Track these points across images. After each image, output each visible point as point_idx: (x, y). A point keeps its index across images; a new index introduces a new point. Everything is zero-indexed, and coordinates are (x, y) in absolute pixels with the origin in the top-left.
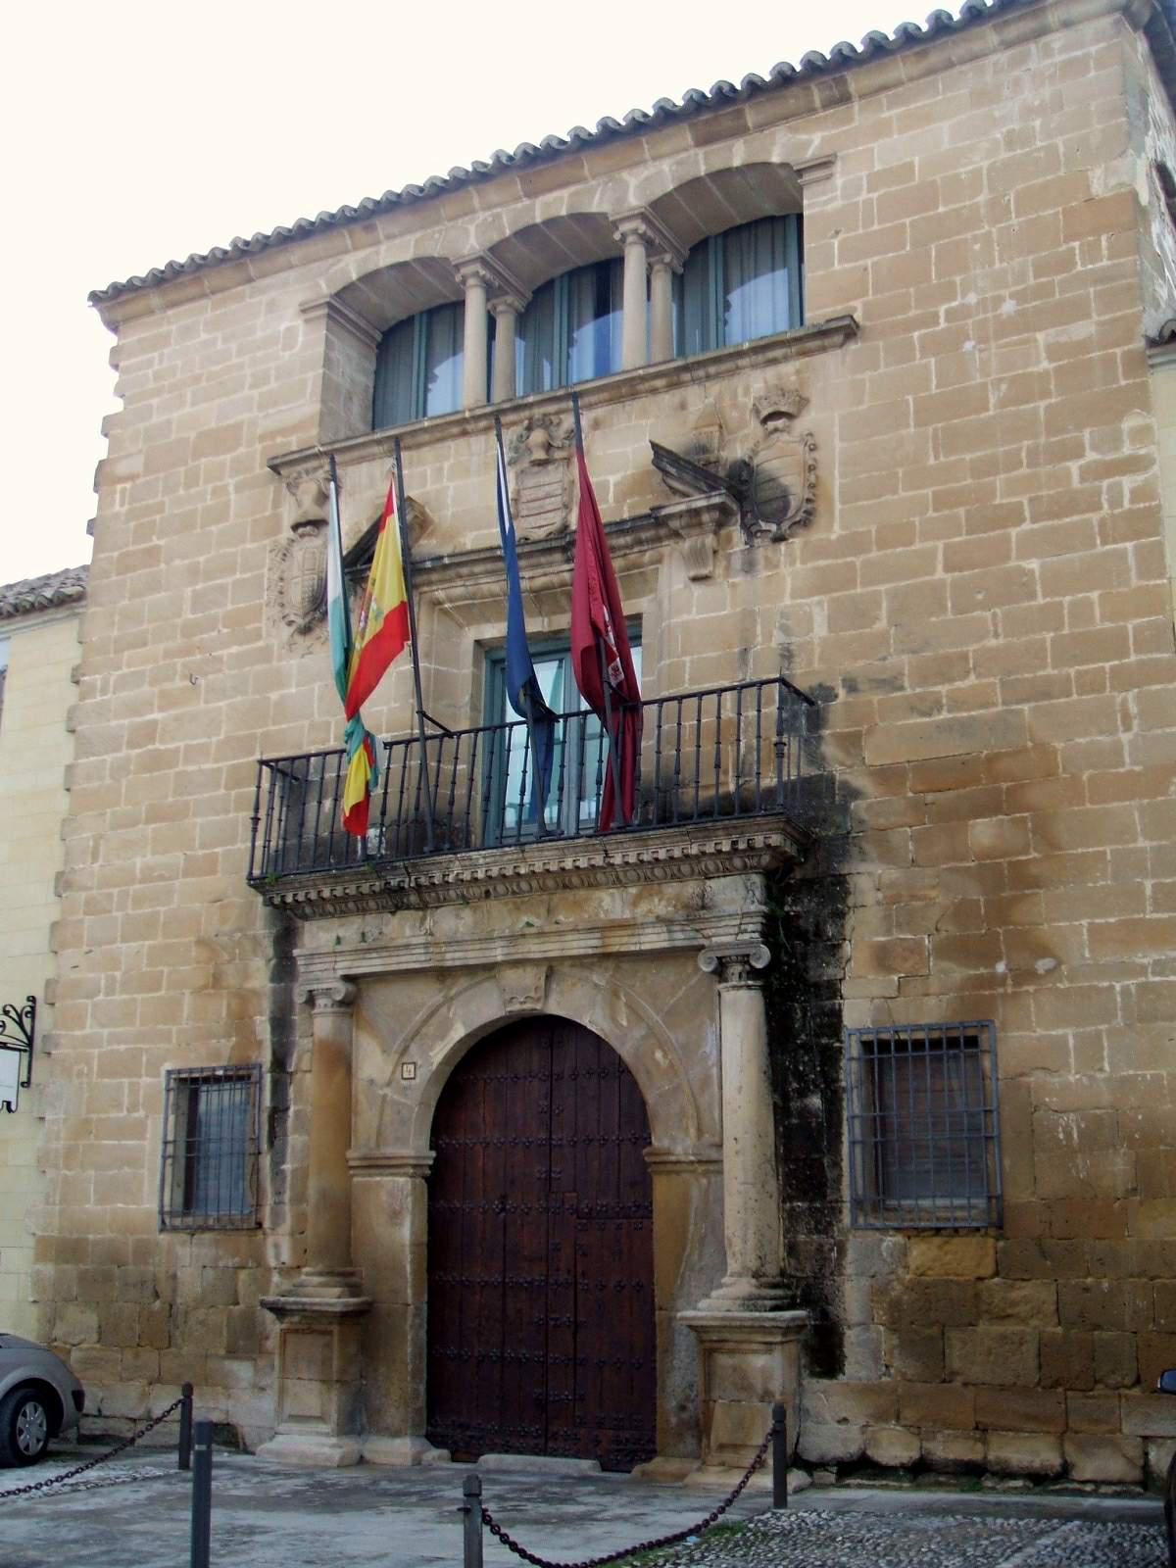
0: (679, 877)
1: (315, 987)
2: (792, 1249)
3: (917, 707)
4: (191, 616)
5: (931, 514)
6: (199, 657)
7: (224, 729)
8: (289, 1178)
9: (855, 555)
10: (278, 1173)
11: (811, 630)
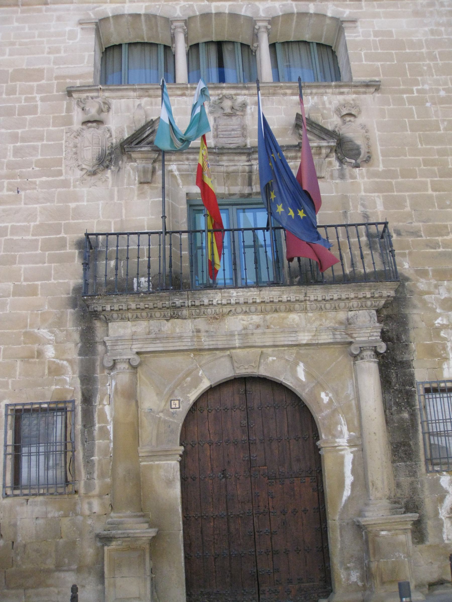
0: (335, 309)
1: (118, 357)
2: (398, 485)
3: (428, 245)
4: (12, 159)
5: (422, 167)
6: (19, 180)
7: (39, 219)
8: (96, 465)
9: (392, 178)
10: (89, 463)
11: (376, 207)
